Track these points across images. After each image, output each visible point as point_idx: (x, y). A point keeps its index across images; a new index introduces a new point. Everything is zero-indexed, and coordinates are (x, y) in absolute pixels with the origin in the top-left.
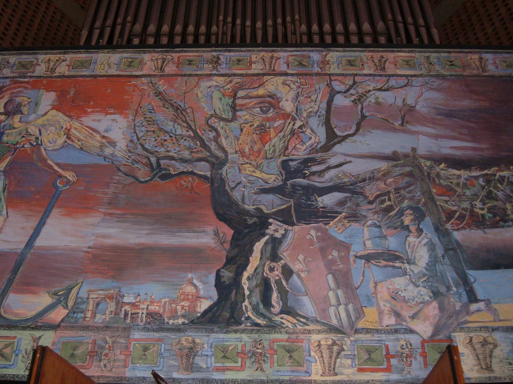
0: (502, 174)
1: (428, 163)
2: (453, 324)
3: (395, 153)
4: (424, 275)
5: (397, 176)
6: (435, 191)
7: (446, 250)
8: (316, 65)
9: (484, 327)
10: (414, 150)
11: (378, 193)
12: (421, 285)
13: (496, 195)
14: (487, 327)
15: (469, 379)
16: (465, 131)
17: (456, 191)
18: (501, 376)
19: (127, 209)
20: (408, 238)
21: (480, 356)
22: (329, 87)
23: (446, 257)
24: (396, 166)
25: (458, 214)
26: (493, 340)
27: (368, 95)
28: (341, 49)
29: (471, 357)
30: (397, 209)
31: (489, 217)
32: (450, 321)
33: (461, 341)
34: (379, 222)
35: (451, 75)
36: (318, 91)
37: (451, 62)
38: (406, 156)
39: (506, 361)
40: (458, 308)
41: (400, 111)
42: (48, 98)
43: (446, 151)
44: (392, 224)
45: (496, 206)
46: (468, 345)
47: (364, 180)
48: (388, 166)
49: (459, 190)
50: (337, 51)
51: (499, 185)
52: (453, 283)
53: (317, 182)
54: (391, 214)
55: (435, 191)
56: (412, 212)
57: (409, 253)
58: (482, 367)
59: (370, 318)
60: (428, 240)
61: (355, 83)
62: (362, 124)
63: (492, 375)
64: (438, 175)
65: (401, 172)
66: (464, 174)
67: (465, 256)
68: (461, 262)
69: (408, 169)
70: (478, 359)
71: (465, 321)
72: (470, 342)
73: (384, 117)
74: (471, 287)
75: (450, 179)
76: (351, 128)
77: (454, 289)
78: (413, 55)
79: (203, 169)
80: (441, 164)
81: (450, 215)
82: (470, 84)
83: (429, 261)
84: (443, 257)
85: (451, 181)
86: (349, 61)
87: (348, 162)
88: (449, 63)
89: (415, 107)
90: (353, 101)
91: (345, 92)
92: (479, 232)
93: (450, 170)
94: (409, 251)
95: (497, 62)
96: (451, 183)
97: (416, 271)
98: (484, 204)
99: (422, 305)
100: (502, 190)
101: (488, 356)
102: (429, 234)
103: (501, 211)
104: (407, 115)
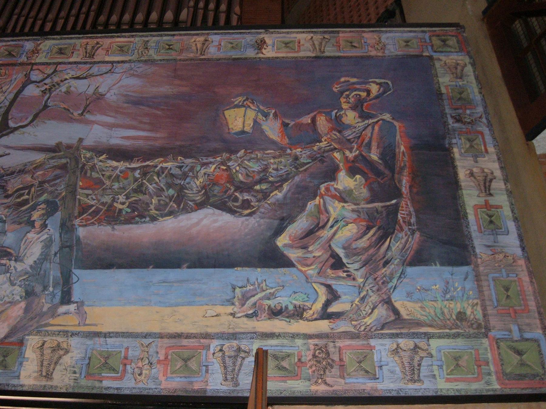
0: (165, 165)
1: (88, 155)
2: (32, 326)
3: (59, 145)
4: (27, 273)
5: (49, 169)
6: (81, 184)
7: (62, 248)
8: (25, 54)
9: (64, 331)
10: (81, 140)
11: (21, 186)
12: (18, 283)
13: (147, 188)
14: (67, 332)
16: (146, 120)
17: (104, 184)
18: (58, 385)
20: (28, 234)
21: (44, 362)
22: (26, 77)
23: (58, 255)
24: (53, 158)
25: (94, 208)
26: (68, 346)
27: (62, 84)
28: (58, 37)
29: (35, 363)
30: (32, 204)
31: (127, 212)
32: (30, 324)
33: (32, 345)
34: (6, 217)
35: (161, 60)
36: (13, 81)
37: (169, 46)
38: (69, 147)
39: (72, 369)
40: (45, 309)
41: (87, 99)
43: (115, 141)
44: (18, 218)
45: (140, 200)
46: (38, 350)
47: (12, 173)
48: (45, 159)
49: (108, 183)
50: (54, 39)
51: (155, 178)
52: (53, 282)
54: (22, 209)
55: (81, 184)
56: (45, 206)
57: (22, 250)
58: (41, 375)
60: (48, 236)
61: (55, 71)
62: (40, 115)
63: (49, 383)
64: (93, 168)
65: (56, 164)
66: (122, 165)
67: (80, 253)
68: (72, 261)
69: (64, 161)
70: (42, 366)
71: (46, 324)
72: (41, 346)
73: (66, 107)
74: (70, 288)
75: (104, 171)
76: (27, 119)
77: (51, 289)
78: (132, 39)
80: (102, 155)
81: (84, 209)
82: (176, 70)
83: (38, 259)
84: (56, 254)
85: (104, 173)
86: (61, 49)
87: (6, 155)
88: (167, 47)
89: (105, 95)
90: (42, 91)
91: (39, 82)
92: (108, 228)
93: (109, 161)
94: (23, 247)
95: (222, 44)
96: (103, 175)
97: (19, 269)
98: (127, 198)
99: (9, 305)
100: (156, 183)
101: (53, 363)
102: (53, 229)
103: (143, 205)
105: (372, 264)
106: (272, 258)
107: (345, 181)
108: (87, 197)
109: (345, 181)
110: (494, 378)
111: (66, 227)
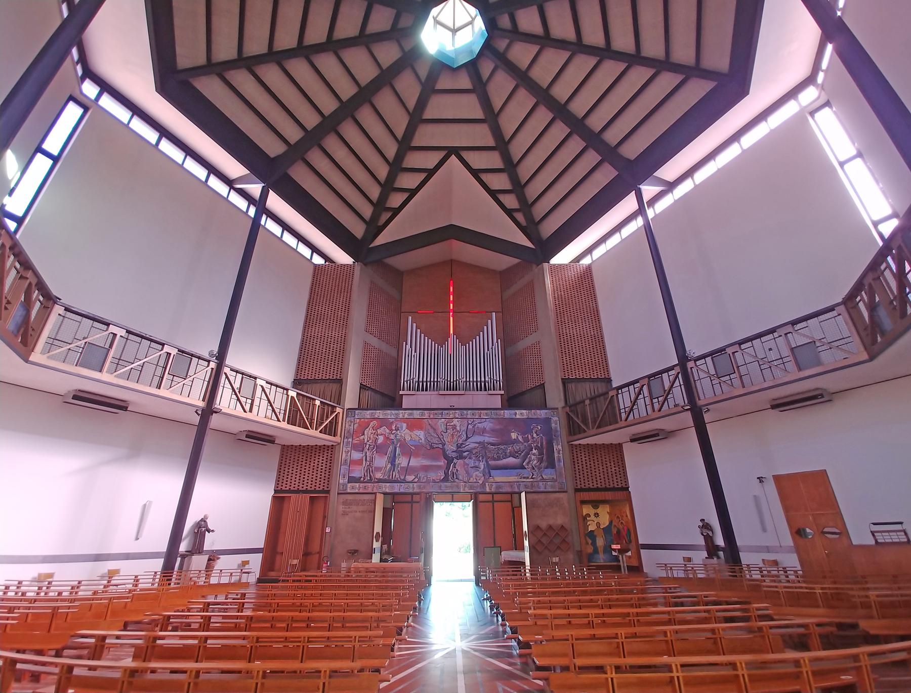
15: (892, 206)
19: (426, 456)
42: (405, 425)
53: (464, 449)
59: (471, 480)
79: (440, 446)
104: (483, 431)
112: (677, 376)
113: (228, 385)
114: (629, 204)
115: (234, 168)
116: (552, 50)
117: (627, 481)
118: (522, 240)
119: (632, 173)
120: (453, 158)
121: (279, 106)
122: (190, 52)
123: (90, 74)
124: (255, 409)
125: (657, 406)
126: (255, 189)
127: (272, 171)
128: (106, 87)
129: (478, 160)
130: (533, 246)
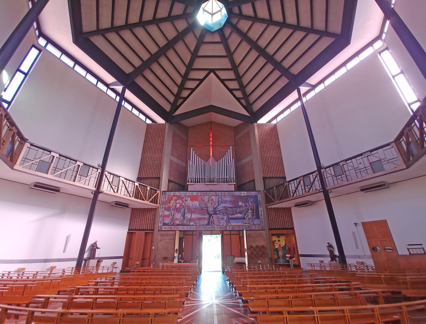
15: (417, 96)
19: (199, 213)
42: (189, 199)
53: (217, 210)
59: (220, 224)
79: (206, 208)
104: (226, 202)
105: (252, 219)
106: (245, 219)
107: (250, 211)
108: (229, 213)
109: (250, 211)
110: (166, 264)
111: (228, 216)
112: (317, 176)
113: (106, 180)
114: (294, 95)
115: (110, 79)
116: (258, 23)
117: (293, 225)
118: (244, 112)
119: (295, 81)
120: (212, 74)
121: (131, 49)
122: (89, 24)
123: (42, 35)
124: (119, 191)
125: (307, 190)
126: (119, 88)
127: (127, 80)
128: (49, 41)
129: (223, 75)
130: (249, 115)
